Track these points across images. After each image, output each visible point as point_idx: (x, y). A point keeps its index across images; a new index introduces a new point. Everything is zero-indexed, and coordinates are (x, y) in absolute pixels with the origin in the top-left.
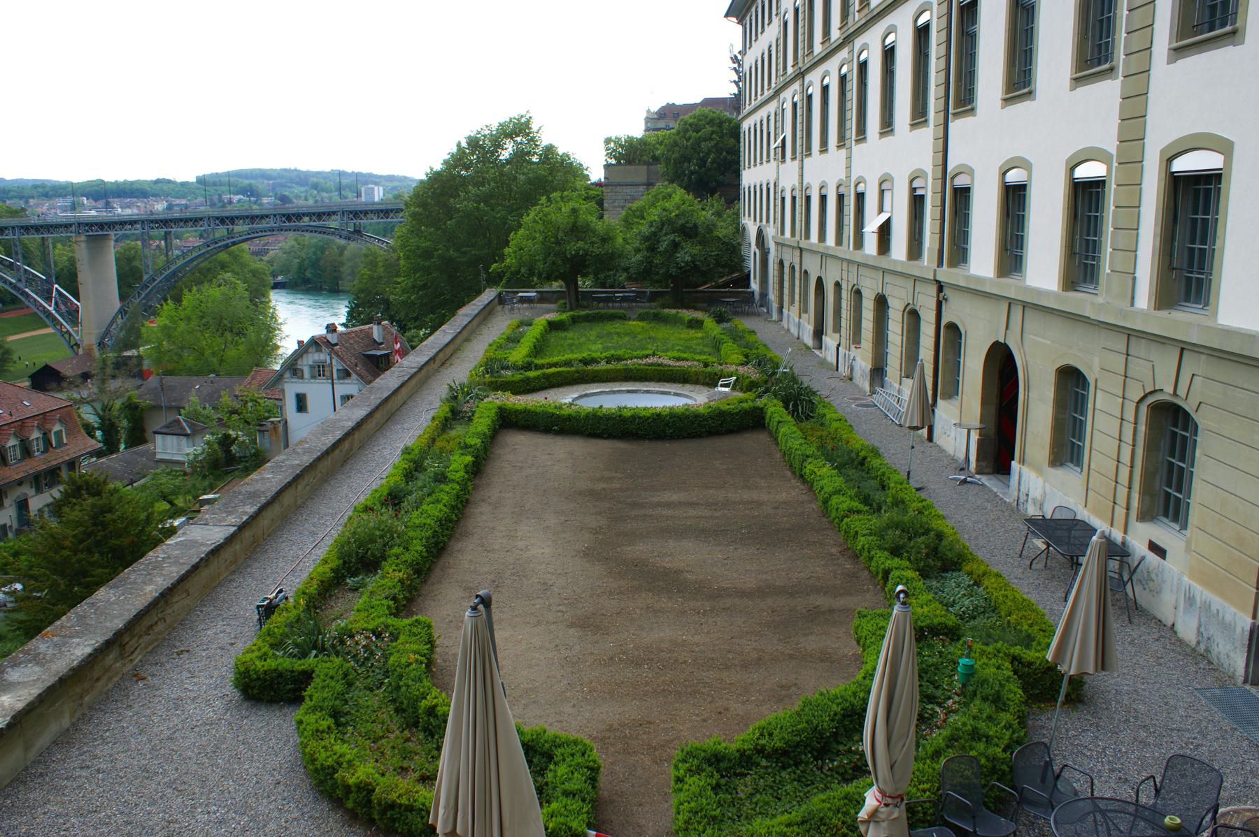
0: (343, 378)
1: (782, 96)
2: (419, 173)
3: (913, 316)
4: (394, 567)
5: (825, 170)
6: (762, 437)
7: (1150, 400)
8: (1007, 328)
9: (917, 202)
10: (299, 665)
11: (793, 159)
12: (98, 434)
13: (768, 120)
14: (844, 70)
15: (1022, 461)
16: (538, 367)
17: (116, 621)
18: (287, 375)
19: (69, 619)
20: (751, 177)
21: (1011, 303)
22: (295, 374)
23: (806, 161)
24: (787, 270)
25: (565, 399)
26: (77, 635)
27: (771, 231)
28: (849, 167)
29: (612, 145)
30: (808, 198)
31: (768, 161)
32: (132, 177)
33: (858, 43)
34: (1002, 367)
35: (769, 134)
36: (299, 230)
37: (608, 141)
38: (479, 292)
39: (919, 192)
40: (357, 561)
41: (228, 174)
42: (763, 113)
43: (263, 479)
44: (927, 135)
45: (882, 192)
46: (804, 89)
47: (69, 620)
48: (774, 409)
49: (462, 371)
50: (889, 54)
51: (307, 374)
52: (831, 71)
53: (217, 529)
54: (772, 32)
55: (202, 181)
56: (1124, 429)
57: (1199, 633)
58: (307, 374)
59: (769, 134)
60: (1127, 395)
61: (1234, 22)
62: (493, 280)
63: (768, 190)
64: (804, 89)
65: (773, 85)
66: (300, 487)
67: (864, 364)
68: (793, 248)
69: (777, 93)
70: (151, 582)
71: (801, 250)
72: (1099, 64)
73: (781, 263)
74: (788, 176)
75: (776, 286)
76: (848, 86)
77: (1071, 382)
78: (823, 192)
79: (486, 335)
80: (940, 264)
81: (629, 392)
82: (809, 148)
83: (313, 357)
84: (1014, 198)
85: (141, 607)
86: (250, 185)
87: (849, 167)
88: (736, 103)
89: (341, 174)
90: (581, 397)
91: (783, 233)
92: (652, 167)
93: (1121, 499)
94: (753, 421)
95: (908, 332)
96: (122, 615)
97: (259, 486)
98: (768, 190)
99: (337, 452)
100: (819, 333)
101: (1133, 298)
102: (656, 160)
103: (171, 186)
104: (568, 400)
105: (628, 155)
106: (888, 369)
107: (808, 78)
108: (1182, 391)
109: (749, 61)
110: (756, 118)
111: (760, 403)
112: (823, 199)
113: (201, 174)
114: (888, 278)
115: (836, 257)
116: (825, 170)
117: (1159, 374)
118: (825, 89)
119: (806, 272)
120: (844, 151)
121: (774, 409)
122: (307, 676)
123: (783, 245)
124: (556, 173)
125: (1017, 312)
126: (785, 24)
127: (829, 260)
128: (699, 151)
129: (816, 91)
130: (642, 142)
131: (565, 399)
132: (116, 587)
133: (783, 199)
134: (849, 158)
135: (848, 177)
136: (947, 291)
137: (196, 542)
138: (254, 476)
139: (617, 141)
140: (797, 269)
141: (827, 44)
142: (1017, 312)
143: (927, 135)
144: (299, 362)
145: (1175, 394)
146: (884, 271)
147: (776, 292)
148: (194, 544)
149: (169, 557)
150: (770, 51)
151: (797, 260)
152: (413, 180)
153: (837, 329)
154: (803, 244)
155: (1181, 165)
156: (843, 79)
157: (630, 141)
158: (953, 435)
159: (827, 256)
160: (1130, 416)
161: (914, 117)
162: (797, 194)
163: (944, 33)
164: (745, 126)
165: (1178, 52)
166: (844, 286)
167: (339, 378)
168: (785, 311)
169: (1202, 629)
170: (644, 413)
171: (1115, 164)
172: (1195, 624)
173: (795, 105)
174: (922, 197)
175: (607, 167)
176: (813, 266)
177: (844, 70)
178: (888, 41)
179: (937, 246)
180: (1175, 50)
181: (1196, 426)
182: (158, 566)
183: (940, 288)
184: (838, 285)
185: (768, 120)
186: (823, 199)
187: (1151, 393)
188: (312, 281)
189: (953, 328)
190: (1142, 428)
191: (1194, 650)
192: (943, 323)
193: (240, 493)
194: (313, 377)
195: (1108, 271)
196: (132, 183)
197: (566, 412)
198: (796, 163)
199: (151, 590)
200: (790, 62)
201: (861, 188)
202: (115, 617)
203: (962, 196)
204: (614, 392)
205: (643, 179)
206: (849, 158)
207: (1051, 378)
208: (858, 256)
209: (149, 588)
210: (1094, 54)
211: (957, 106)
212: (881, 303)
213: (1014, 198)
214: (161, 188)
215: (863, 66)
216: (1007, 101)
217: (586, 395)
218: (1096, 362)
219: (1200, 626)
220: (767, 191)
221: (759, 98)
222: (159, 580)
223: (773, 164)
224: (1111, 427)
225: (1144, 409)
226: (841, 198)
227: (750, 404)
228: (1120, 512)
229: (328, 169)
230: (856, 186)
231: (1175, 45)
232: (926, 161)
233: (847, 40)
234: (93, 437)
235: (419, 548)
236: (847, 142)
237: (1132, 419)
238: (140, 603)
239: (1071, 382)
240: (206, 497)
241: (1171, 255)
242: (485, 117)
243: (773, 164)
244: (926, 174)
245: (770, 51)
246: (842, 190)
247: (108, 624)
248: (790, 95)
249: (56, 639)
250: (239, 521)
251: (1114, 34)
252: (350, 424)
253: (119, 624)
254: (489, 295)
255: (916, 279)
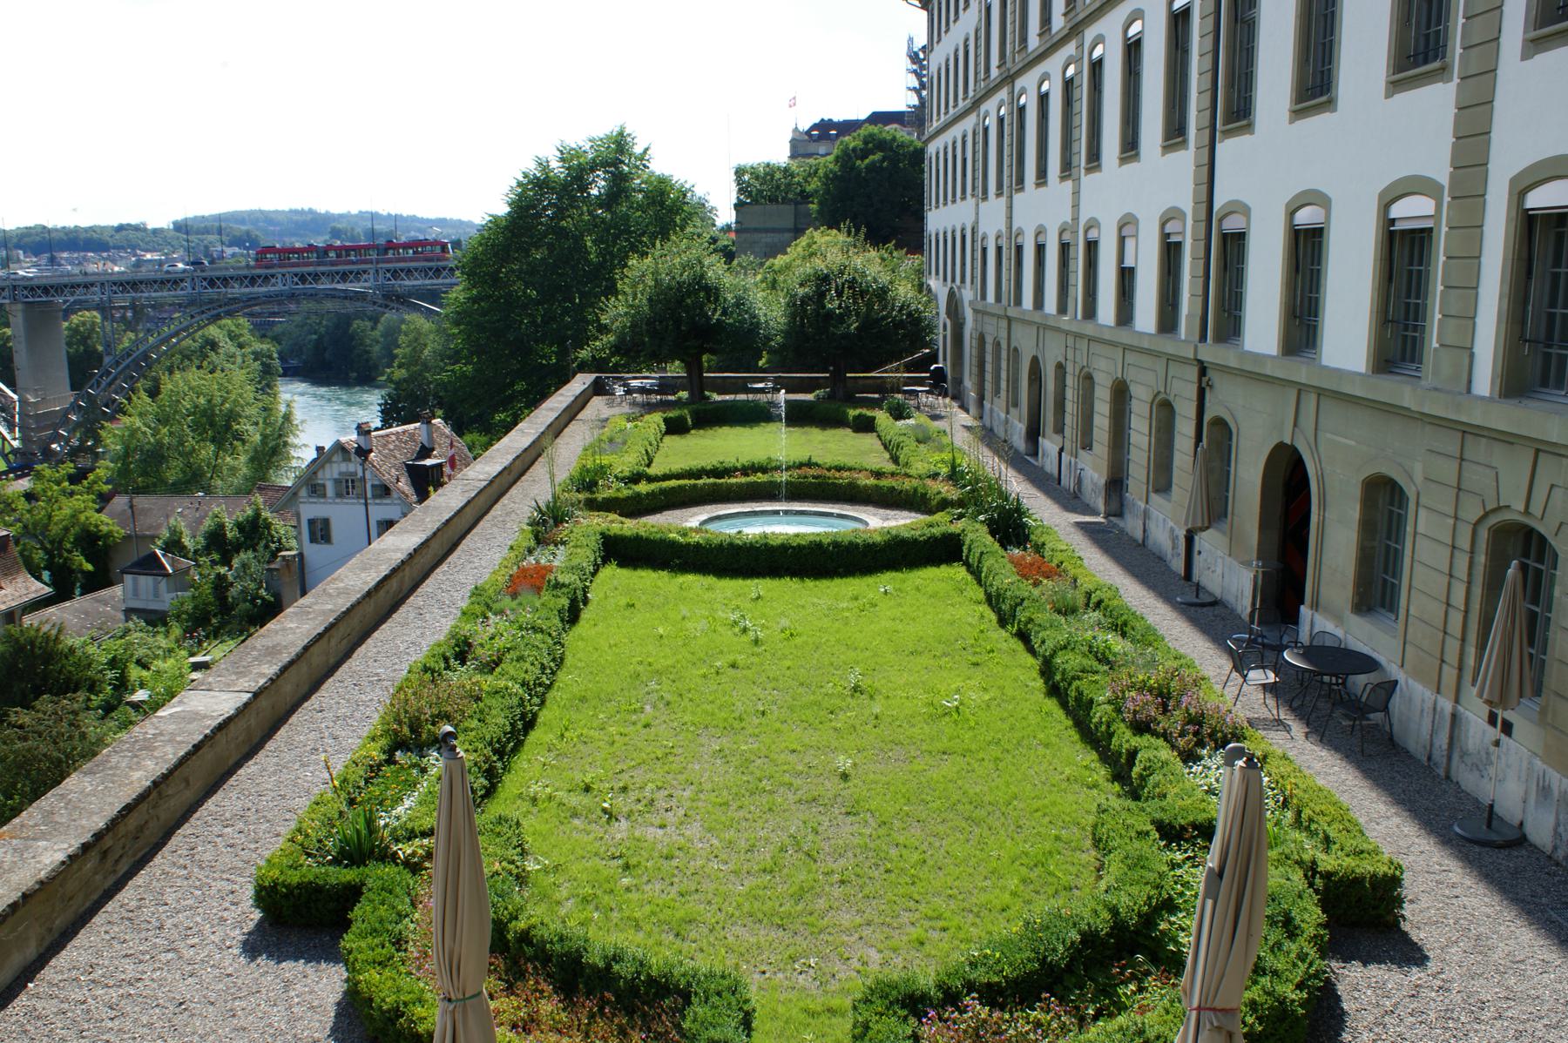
0: (380, 497)
1: (983, 108)
2: (503, 209)
3: (1165, 411)
4: (467, 746)
5: (1042, 209)
6: (958, 572)
7: (1493, 520)
8: (1295, 425)
9: (1171, 252)
10: (349, 875)
11: (999, 194)
12: (46, 575)
13: (964, 143)
14: (1071, 71)
15: (1316, 606)
16: (651, 479)
17: (95, 818)
18: (303, 492)
19: (31, 816)
20: (939, 220)
21: (1301, 389)
22: (314, 492)
23: (1017, 197)
24: (989, 348)
25: (690, 523)
26: (44, 836)
27: (967, 294)
28: (1076, 206)
29: (746, 177)
30: (1019, 249)
31: (964, 198)
32: (85, 223)
33: (1090, 34)
34: (1290, 483)
35: (964, 160)
36: (314, 295)
37: (739, 172)
38: (564, 380)
39: (1173, 239)
40: (409, 737)
41: (219, 218)
42: (956, 132)
43: (284, 629)
44: (1186, 160)
45: (1122, 241)
46: (1014, 99)
47: (31, 816)
48: (977, 534)
49: (537, 489)
50: (1133, 50)
51: (330, 491)
52: (1052, 73)
53: (224, 696)
54: (969, 21)
55: (182, 227)
56: (1456, 561)
57: (1557, 834)
58: (330, 491)
59: (964, 160)
60: (1461, 514)
61: (1444, 57)
62: (583, 367)
63: (963, 237)
64: (1014, 99)
65: (971, 93)
66: (333, 642)
67: (1096, 476)
68: (999, 317)
69: (976, 104)
70: (139, 766)
71: (1010, 320)
72: (1426, 62)
73: (982, 340)
74: (991, 218)
75: (975, 370)
76: (1076, 95)
77: (1384, 501)
78: (1041, 239)
79: (594, 429)
80: (1203, 338)
81: (786, 512)
82: (1021, 180)
83: (336, 469)
84: (1306, 248)
85: (129, 800)
86: (248, 233)
87: (1076, 206)
88: (916, 118)
89: (374, 216)
90: (711, 520)
91: (984, 297)
92: (801, 207)
93: (1452, 656)
94: (945, 550)
95: (1158, 430)
96: (101, 810)
97: (278, 638)
98: (963, 237)
99: (382, 593)
100: (1034, 433)
101: (1470, 382)
102: (805, 197)
103: (140, 234)
104: (693, 522)
105: (761, 191)
106: (1131, 483)
107: (1020, 83)
108: (1537, 509)
109: (936, 60)
110: (947, 137)
111: (957, 527)
112: (1040, 249)
113: (179, 217)
114: (1131, 358)
115: (1058, 330)
116: (1042, 209)
117: (1509, 487)
118: (1043, 99)
119: (1016, 350)
120: (1069, 184)
121: (977, 534)
122: (353, 893)
123: (984, 313)
124: (668, 210)
125: (1310, 402)
126: (988, 9)
127: (1049, 334)
128: (867, 180)
129: (1030, 101)
130: (786, 171)
131: (690, 523)
132: (91, 772)
133: (984, 250)
134: (1076, 193)
135: (1076, 219)
136: (1210, 373)
137: (197, 713)
138: (271, 625)
139: (753, 171)
140: (1004, 345)
141: (1047, 37)
142: (1310, 402)
143: (1186, 160)
144: (320, 475)
145: (1527, 512)
146: (1126, 348)
147: (975, 379)
148: (196, 716)
149: (161, 734)
150: (966, 46)
151: (1003, 334)
152: (470, 224)
153: (1059, 429)
154: (1012, 312)
155: (1539, 199)
156: (1068, 85)
157: (770, 170)
158: (1219, 571)
159: (1046, 327)
160: (1464, 542)
161: (1063, 171)
162: (1004, 242)
163: (1210, 20)
164: (931, 149)
165: (1535, 45)
166: (1069, 369)
167: (374, 497)
168: (987, 404)
169: (1561, 829)
170: (798, 540)
171: (1447, 199)
172: (1552, 820)
173: (1001, 120)
174: (1179, 245)
175: (739, 206)
176: (1026, 342)
177: (1071, 71)
178: (1132, 31)
179: (1199, 312)
180: (1532, 41)
181: (1556, 555)
182: (148, 746)
183: (1203, 371)
184: (1061, 368)
185: (964, 143)
186: (1040, 249)
187: (1494, 511)
188: (333, 362)
189: (1220, 423)
190: (1481, 559)
191: (1550, 857)
192: (1207, 418)
193: (254, 648)
194: (339, 495)
195: (1435, 345)
196: (86, 230)
197: (696, 538)
198: (1003, 200)
199: (140, 777)
200: (995, 61)
201: (1093, 234)
202: (92, 813)
203: (1233, 247)
204: (755, 514)
205: (790, 223)
206: (1076, 193)
207: (1356, 492)
208: (1088, 329)
209: (136, 775)
210: (1418, 50)
211: (1227, 121)
212: (1121, 394)
213: (1306, 248)
214: (128, 237)
215: (1097, 67)
216: (1298, 113)
217: (719, 518)
218: (1419, 467)
219: (1557, 825)
220: (968, 238)
221: (951, 111)
222: (150, 764)
223: (970, 201)
224: (1436, 559)
225: (1484, 534)
226: (1064, 248)
227: (943, 529)
228: (1450, 674)
229: (354, 211)
230: (1086, 232)
231: (1533, 34)
232: (1185, 198)
233: (1075, 30)
234: (39, 578)
235: (501, 721)
236: (1074, 171)
237: (1467, 547)
238: (127, 795)
239: (1384, 501)
240: (810, 397)
241: (1523, 322)
242: (584, 131)
243: (970, 201)
244: (1184, 214)
245: (966, 46)
246: (1067, 237)
247: (84, 822)
248: (994, 108)
249: (14, 842)
250: (254, 687)
251: (1447, 20)
252: (401, 556)
253: (100, 823)
254: (580, 383)
255: (1171, 359)
